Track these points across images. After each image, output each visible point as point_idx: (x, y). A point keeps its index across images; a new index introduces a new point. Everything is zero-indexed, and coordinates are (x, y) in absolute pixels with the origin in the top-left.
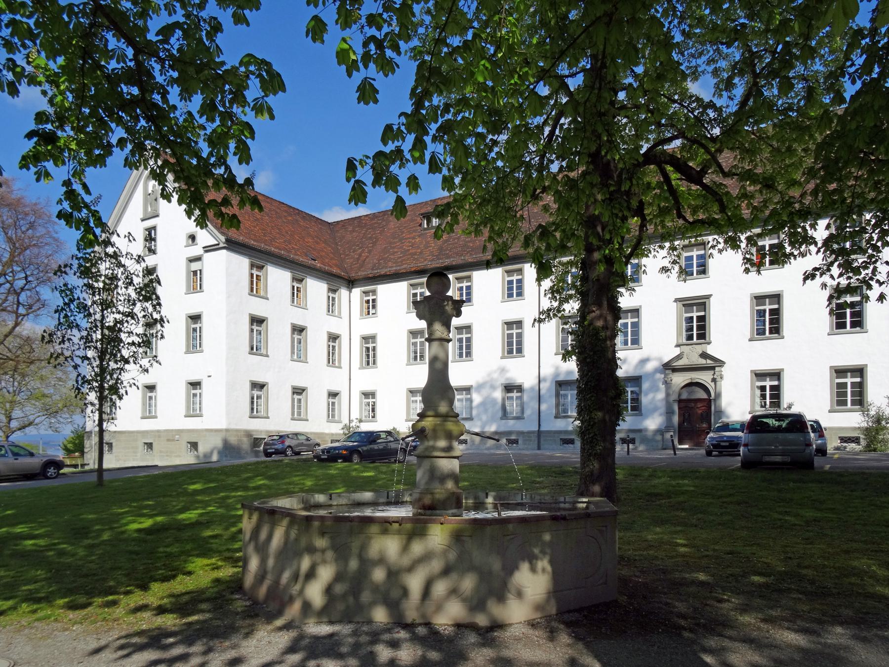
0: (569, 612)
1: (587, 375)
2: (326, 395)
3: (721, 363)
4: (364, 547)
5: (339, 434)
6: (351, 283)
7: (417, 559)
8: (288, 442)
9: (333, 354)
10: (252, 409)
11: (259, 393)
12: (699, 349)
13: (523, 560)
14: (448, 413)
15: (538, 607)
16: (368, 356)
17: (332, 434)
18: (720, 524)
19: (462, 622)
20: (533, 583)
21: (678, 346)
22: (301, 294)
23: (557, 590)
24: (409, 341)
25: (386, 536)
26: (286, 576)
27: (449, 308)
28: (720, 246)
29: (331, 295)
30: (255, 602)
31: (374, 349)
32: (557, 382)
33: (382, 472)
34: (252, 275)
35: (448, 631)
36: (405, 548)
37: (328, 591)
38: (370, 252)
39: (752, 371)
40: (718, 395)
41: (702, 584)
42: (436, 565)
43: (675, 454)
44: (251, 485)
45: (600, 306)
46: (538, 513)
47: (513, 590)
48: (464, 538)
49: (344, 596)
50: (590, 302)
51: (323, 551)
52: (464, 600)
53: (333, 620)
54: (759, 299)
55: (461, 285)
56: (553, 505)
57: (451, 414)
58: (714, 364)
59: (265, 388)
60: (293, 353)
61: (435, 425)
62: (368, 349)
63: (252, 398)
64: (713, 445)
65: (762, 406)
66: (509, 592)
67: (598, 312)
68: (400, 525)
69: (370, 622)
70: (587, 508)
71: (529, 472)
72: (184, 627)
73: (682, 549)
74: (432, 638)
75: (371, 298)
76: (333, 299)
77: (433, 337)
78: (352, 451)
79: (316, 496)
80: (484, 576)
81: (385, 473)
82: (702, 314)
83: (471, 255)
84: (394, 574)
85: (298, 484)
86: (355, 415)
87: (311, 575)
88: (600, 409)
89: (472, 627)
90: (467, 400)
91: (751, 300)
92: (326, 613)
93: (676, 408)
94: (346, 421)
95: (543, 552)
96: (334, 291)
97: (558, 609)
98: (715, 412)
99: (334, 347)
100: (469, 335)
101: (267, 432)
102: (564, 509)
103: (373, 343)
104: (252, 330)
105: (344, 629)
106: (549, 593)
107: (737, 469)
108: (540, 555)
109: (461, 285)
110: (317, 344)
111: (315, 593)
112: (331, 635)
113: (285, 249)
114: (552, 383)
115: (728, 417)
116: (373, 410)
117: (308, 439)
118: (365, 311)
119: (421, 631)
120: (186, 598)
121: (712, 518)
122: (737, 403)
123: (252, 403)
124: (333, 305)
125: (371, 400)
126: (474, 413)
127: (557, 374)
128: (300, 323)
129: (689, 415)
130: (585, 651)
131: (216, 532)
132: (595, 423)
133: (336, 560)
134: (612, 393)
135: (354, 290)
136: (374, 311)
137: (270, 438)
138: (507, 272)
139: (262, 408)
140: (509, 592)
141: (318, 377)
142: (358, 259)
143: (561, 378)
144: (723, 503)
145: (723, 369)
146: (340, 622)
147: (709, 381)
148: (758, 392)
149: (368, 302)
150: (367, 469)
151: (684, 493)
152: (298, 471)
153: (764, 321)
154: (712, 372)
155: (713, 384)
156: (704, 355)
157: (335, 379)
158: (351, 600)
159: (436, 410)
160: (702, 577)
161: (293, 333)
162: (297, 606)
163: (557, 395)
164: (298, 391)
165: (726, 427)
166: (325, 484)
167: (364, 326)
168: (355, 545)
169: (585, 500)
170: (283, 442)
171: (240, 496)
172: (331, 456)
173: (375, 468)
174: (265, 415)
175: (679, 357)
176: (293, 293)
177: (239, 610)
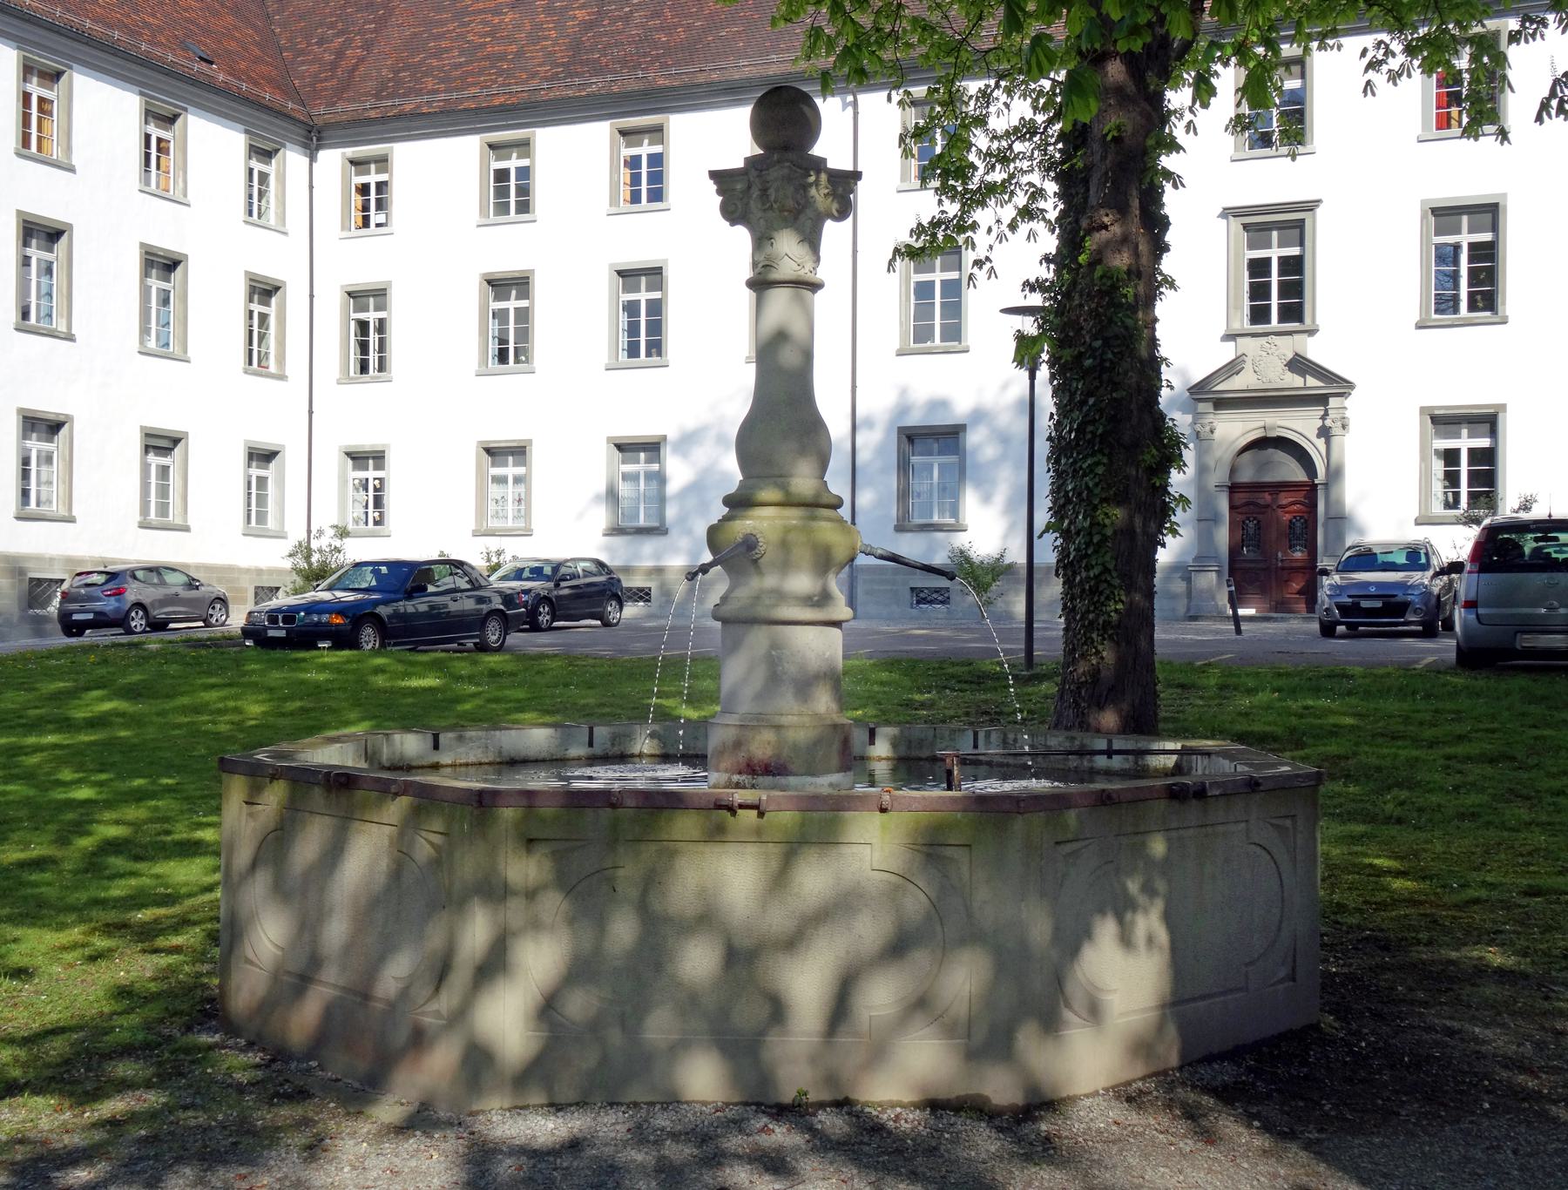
0: (1209, 1059)
1: (1083, 402)
2: (241, 457)
3: (1343, 386)
4: (652, 881)
5: (280, 572)
6: (313, 139)
7: (822, 918)
8: (133, 593)
9: (262, 337)
10: (25, 494)
11: (46, 446)
12: (1286, 347)
13: (1102, 911)
14: (818, 495)
15: (1141, 1047)
16: (364, 347)
17: (259, 572)
18: (1462, 816)
19: (943, 1094)
20: (1125, 975)
21: (1230, 337)
22: (171, 160)
23: (1180, 1002)
24: (484, 308)
25: (718, 848)
26: (397, 971)
27: (819, 195)
28: (1394, 64)
29: (257, 166)
30: (279, 1055)
31: (382, 326)
32: (901, 430)
33: (459, 678)
34: (26, 97)
35: (911, 1121)
36: (779, 880)
37: (548, 1009)
38: (368, 46)
39: (1423, 410)
40: (1335, 474)
41: (1502, 974)
42: (869, 931)
43: (1238, 631)
44: (80, 714)
45: (1122, 210)
46: (1008, 786)
47: (1078, 1001)
48: (949, 852)
49: (595, 1027)
50: (1093, 201)
51: (531, 895)
52: (951, 1031)
53: (560, 1099)
54: (1444, 215)
55: (634, 151)
56: (1073, 762)
57: (825, 500)
58: (1323, 389)
59: (64, 431)
60: (145, 331)
61: (787, 530)
62: (363, 326)
63: (26, 461)
64: (1340, 607)
65: (1447, 506)
66: (1068, 1006)
67: (1116, 229)
68: (761, 815)
69: (672, 1101)
70: (1178, 769)
71: (884, 676)
72: (99, 1136)
73: (1398, 884)
74: (867, 1140)
75: (372, 178)
76: (264, 177)
77: (775, 276)
78: (358, 617)
79: (397, 737)
80: (1010, 960)
81: (471, 679)
82: (1295, 251)
83: (665, 66)
84: (742, 958)
85: (220, 712)
86: (326, 517)
87: (494, 965)
88: (1120, 499)
89: (976, 1108)
90: (649, 476)
91: (1424, 217)
92: (538, 1079)
93: (1223, 504)
94: (297, 533)
95: (1149, 890)
96: (267, 155)
97: (1183, 1054)
98: (1328, 518)
99: (263, 318)
100: (656, 295)
101: (70, 561)
102: (1109, 774)
103: (380, 307)
104: (25, 262)
105: (609, 1126)
106: (1163, 1006)
107: (1450, 670)
108: (1142, 899)
109: (634, 151)
110: (213, 303)
111: (506, 1020)
112: (574, 1145)
113: (123, 27)
114: (888, 431)
115: (1361, 532)
116: (378, 503)
117: (192, 584)
118: (356, 216)
119: (832, 1123)
120: (56, 1048)
121: (1434, 799)
122: (1387, 499)
123: (25, 474)
124: (261, 194)
125: (371, 474)
126: (671, 512)
127: (903, 409)
128: (168, 242)
129: (1258, 526)
130: (1322, 1168)
131: (35, 852)
132: (1105, 539)
133: (571, 921)
134: (1150, 456)
135: (323, 154)
136: (381, 218)
137: (79, 581)
138: (624, 133)
139: (55, 491)
140: (1068, 1006)
141: (216, 402)
142: (334, 66)
143: (914, 420)
144: (1448, 758)
145: (1348, 402)
146: (581, 1104)
147: (1312, 435)
148: (1439, 467)
149: (364, 190)
150: (412, 670)
151: (1335, 732)
152: (209, 674)
153: (1455, 276)
154: (1320, 411)
155: (1321, 443)
156: (1299, 364)
157: (270, 412)
158: (615, 1037)
159: (784, 488)
160: (1496, 957)
161: (146, 274)
162: (441, 1060)
163: (904, 467)
164: (161, 443)
165: (1366, 559)
166: (303, 710)
167: (357, 259)
168: (628, 871)
169: (1170, 745)
170: (119, 593)
171: (55, 746)
172: (289, 633)
173: (437, 666)
174: (63, 512)
175: (1233, 368)
176: (147, 156)
177: (242, 1077)
